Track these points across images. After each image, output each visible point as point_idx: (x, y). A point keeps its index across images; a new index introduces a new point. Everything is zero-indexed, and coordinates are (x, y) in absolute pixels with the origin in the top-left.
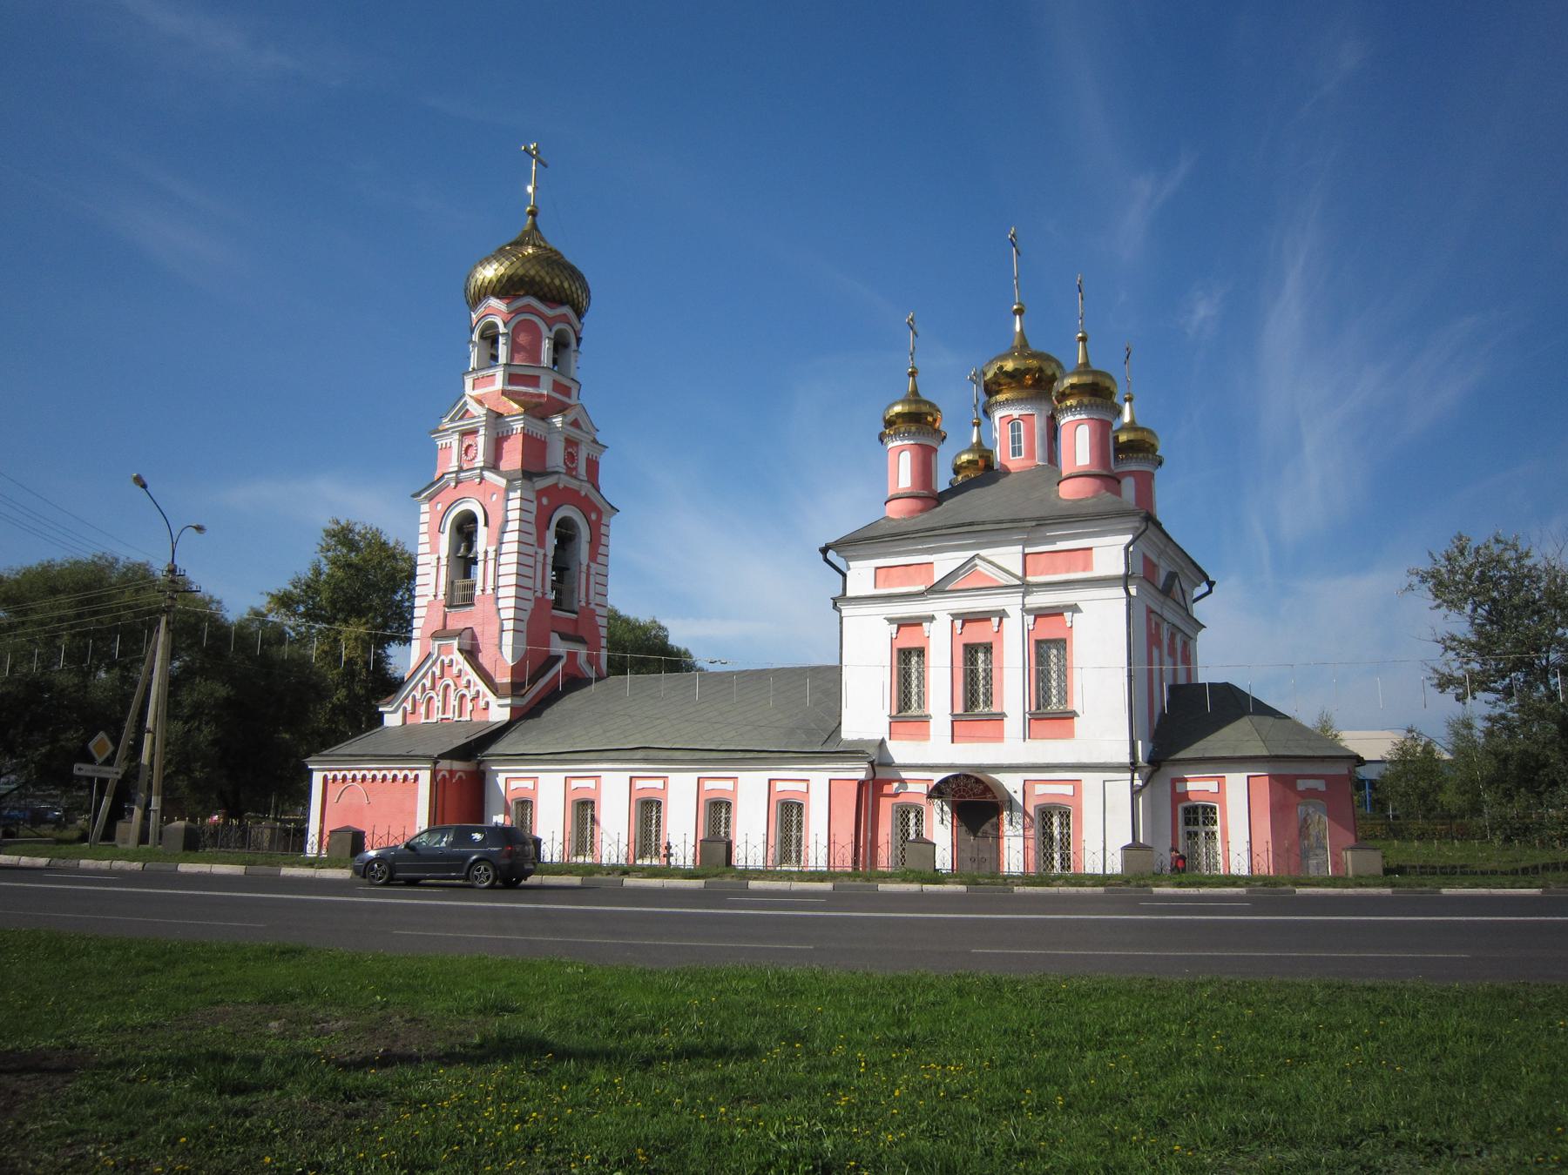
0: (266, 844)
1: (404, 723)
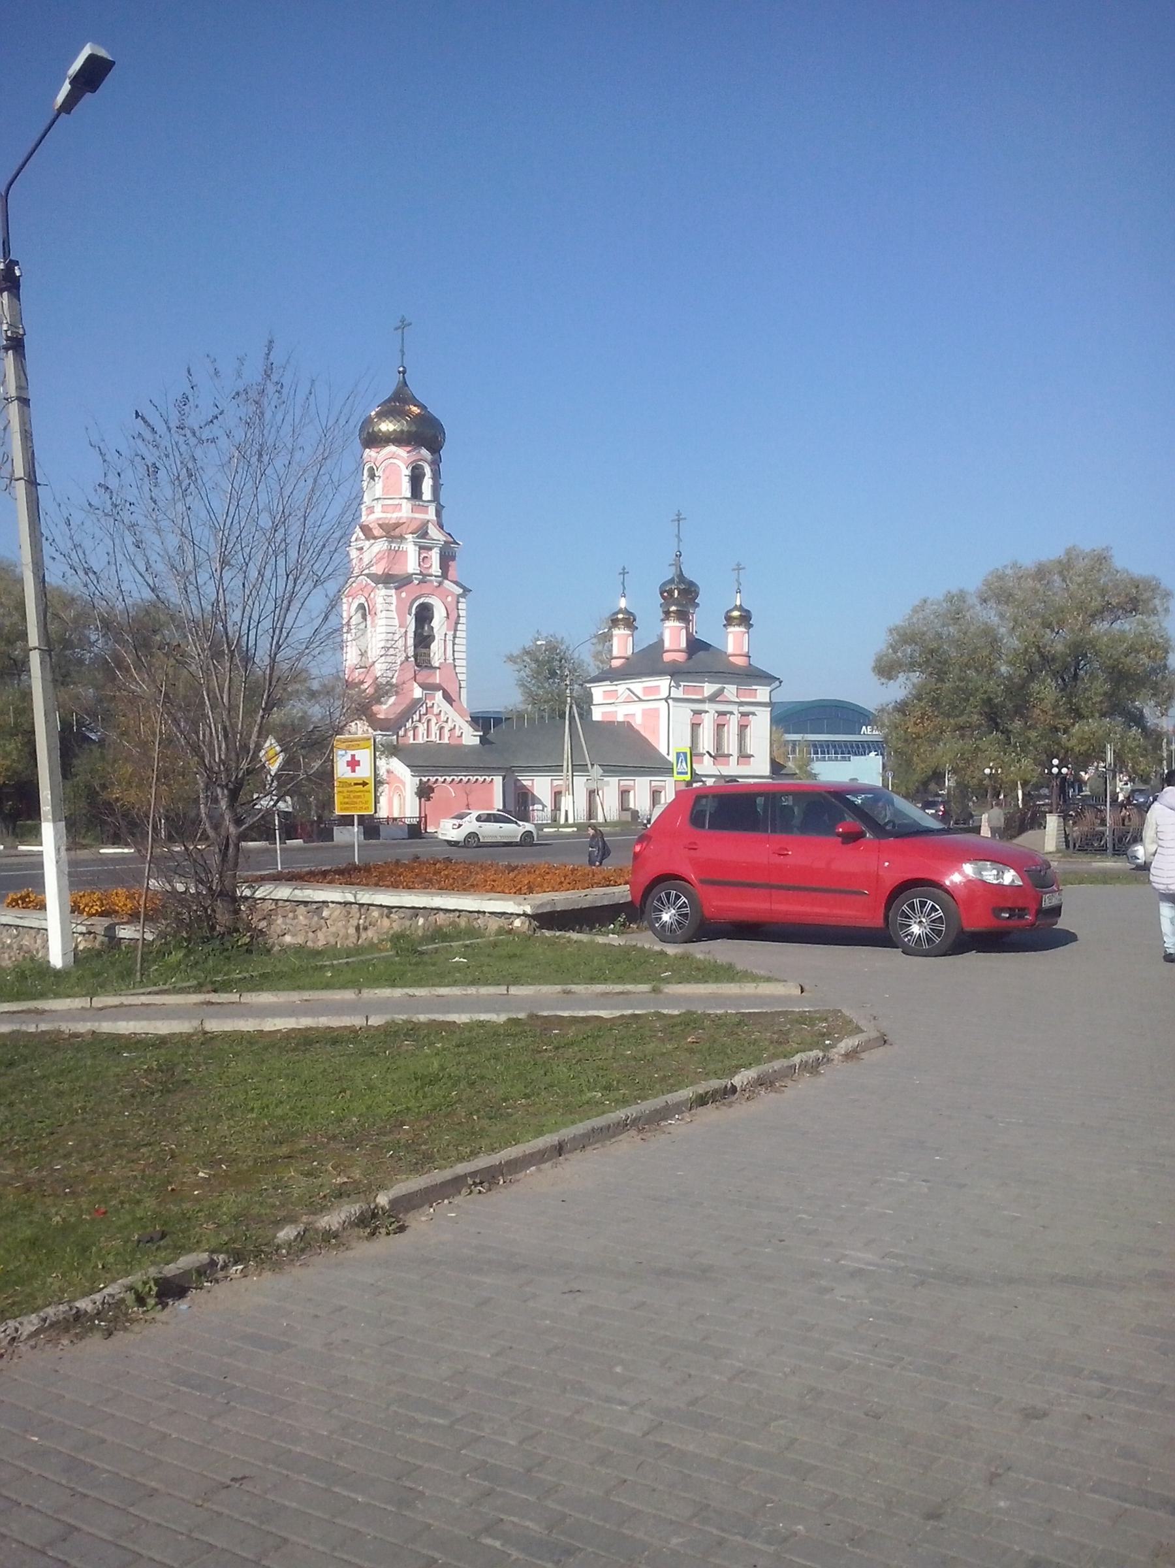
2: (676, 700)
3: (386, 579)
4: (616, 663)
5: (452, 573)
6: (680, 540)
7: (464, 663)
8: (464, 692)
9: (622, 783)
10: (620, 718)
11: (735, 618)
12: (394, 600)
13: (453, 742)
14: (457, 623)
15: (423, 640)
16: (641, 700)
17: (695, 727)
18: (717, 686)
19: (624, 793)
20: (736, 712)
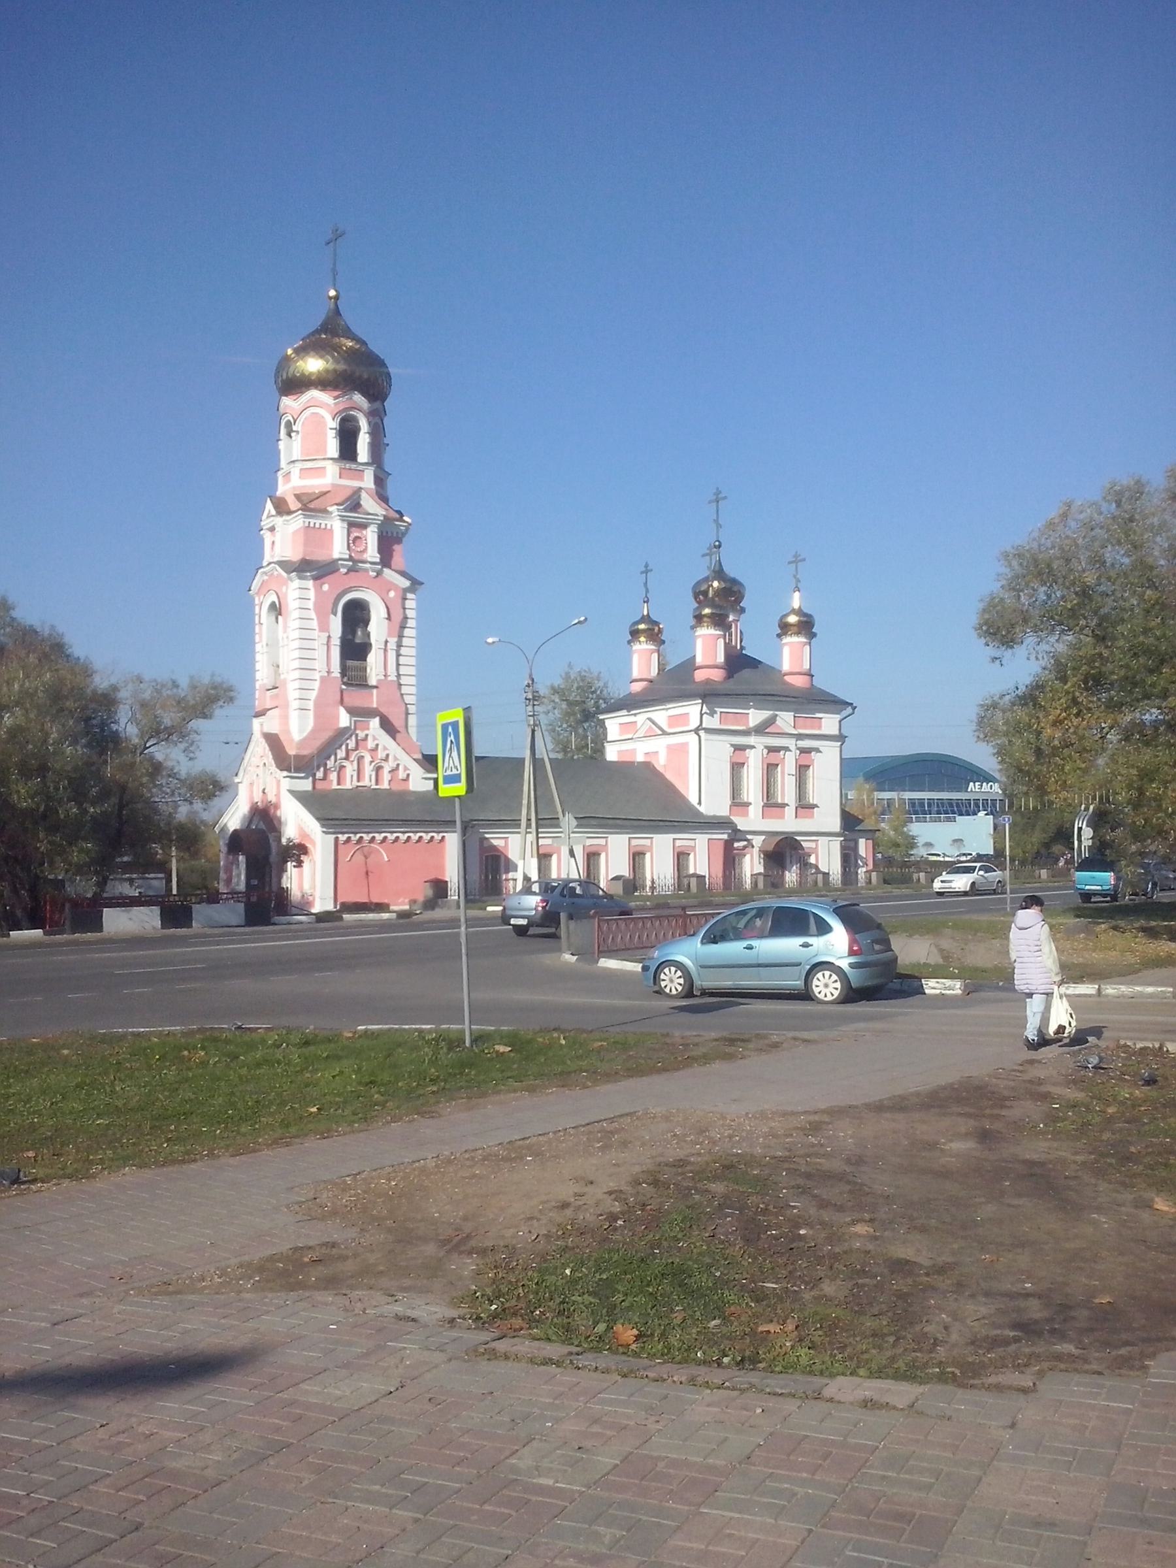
0: (67, 905)
1: (314, 787)
2: (709, 731)
3: (303, 567)
4: (637, 687)
5: (398, 559)
6: (719, 526)
7: (413, 680)
8: (412, 720)
9: (634, 842)
10: (640, 758)
11: (792, 625)
12: (311, 594)
13: (396, 787)
14: (403, 627)
15: (354, 650)
16: (664, 733)
17: (737, 767)
18: (765, 714)
19: (637, 857)
20: (793, 748)
